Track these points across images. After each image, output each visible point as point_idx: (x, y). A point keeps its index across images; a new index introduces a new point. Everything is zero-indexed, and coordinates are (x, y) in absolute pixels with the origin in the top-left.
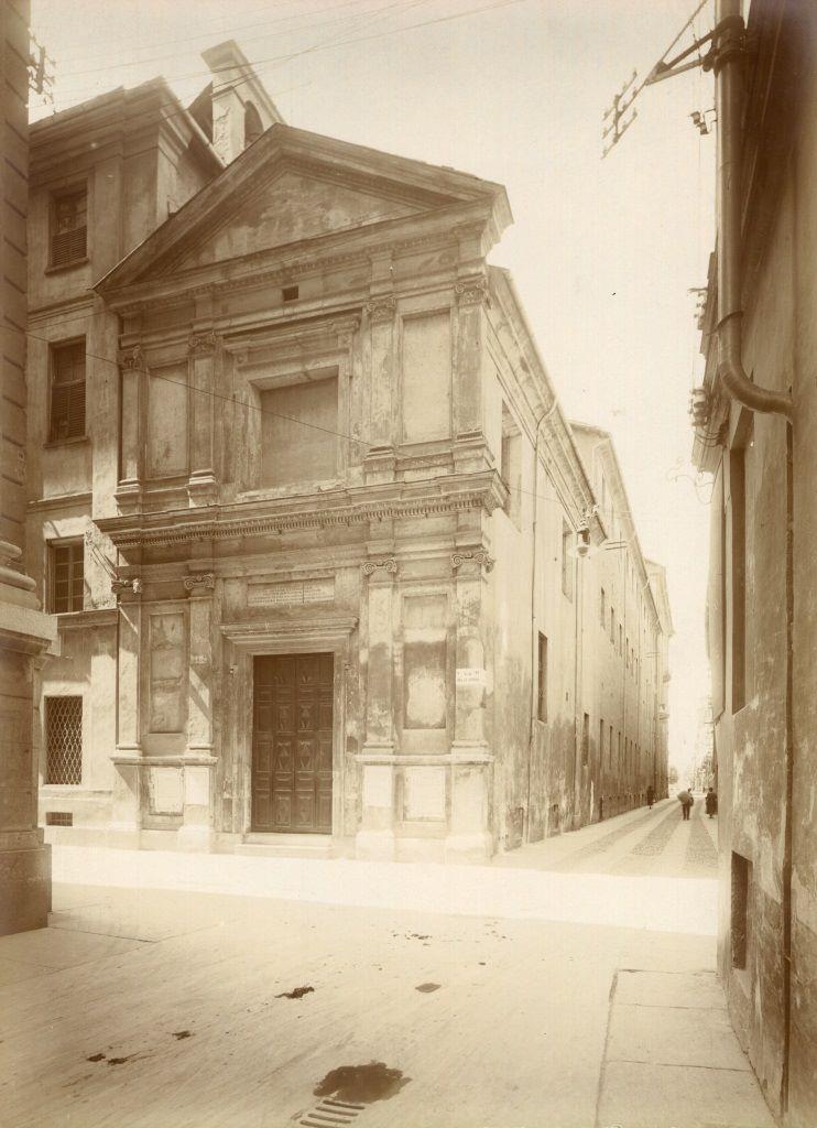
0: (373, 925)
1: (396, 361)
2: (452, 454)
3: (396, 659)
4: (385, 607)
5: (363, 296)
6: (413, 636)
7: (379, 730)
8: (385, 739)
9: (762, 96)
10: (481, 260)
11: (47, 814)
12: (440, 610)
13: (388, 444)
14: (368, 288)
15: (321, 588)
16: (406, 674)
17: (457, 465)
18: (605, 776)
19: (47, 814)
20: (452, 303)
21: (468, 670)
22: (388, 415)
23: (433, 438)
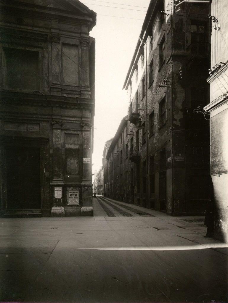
0: (131, 227)
1: (60, 57)
2: (80, 91)
3: (63, 153)
4: (59, 136)
5: (48, 31)
6: (68, 146)
7: (58, 176)
8: (60, 178)
9: (180, 2)
10: (89, 34)
11: (38, 52)
12: (76, 139)
13: (58, 83)
14: (50, 29)
15: (34, 126)
16: (66, 158)
17: (82, 95)
18: (40, 213)
19: (38, 52)
20: (79, 44)
21: (87, 158)
22: (58, 74)
23: (73, 85)
